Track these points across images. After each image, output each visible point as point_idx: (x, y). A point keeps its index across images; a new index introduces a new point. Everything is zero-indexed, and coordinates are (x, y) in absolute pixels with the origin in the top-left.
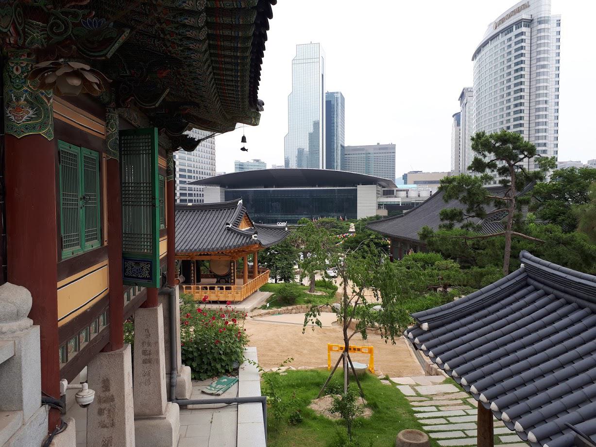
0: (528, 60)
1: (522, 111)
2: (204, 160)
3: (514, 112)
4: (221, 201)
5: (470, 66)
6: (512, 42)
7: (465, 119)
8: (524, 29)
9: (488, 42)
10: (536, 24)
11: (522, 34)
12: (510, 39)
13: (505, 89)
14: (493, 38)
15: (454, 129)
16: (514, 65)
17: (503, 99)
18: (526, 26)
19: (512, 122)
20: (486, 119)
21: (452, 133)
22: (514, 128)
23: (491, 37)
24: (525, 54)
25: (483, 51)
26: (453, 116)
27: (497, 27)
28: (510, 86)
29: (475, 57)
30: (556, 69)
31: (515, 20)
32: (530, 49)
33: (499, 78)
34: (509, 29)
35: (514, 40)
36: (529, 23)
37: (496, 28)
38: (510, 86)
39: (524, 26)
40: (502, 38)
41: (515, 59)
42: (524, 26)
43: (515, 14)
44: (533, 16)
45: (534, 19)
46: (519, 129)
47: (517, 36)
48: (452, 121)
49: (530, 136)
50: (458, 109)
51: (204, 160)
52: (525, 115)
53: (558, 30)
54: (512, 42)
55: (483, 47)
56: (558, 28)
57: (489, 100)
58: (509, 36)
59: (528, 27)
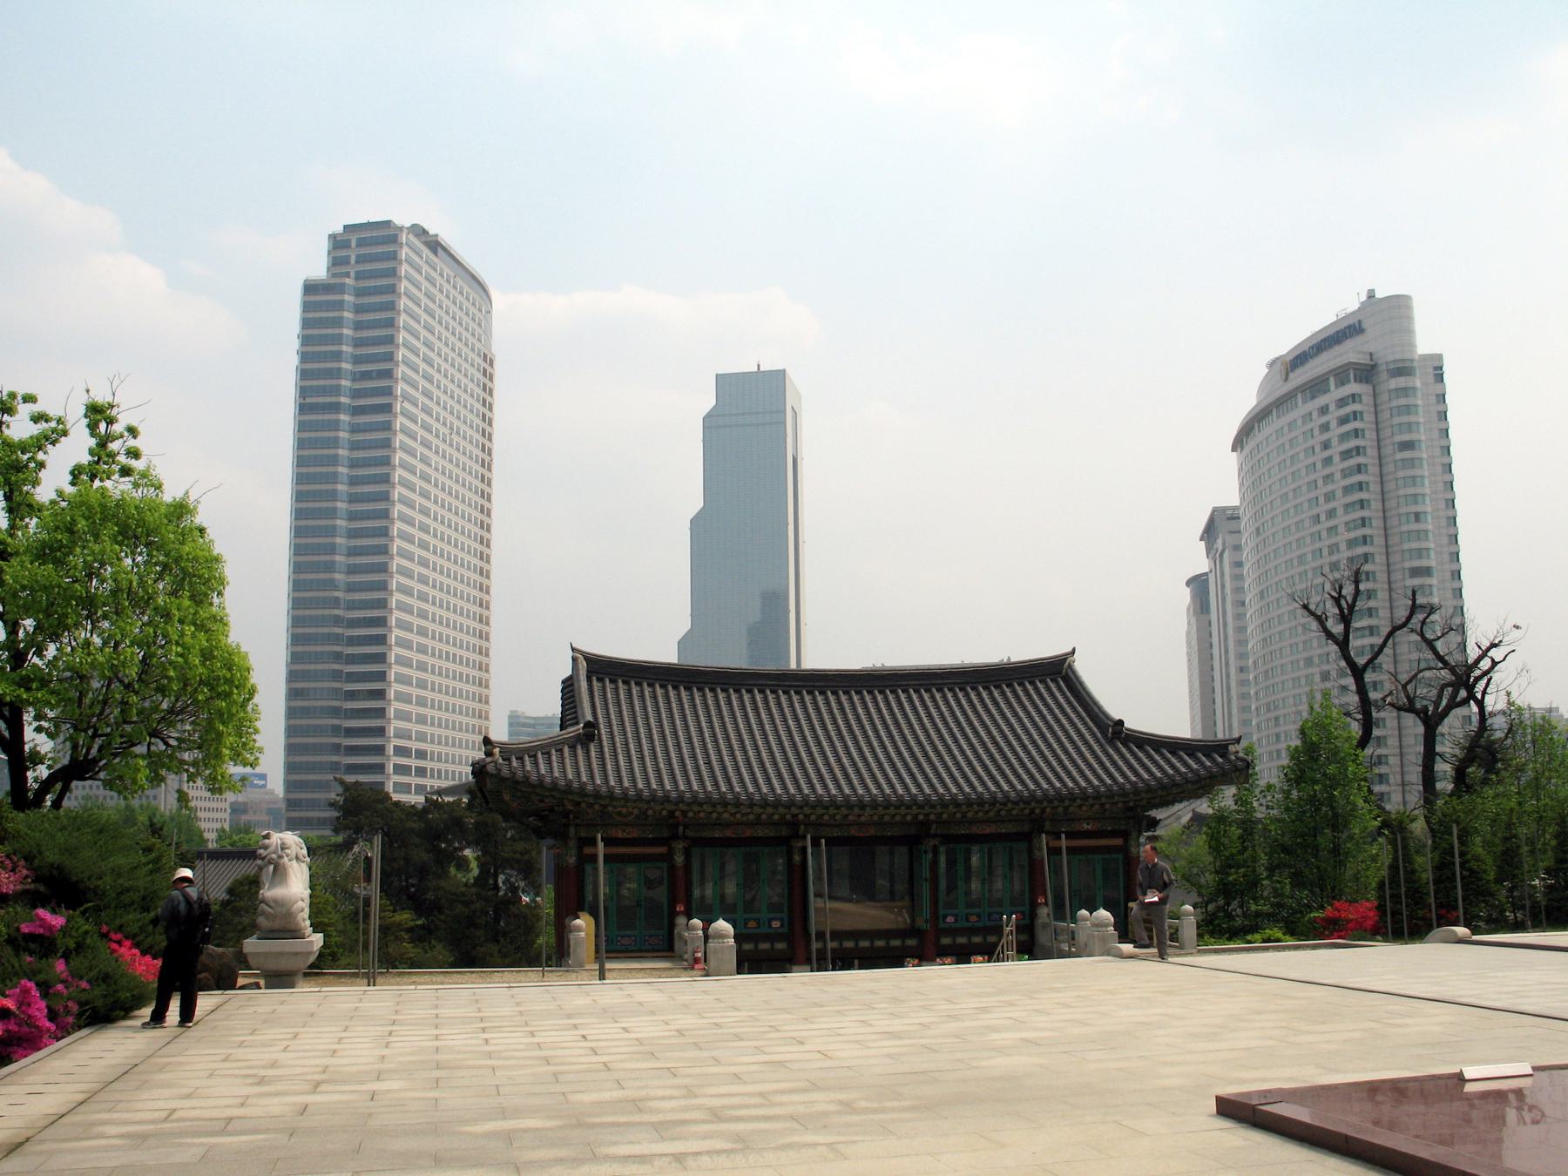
0: (1373, 465)
1: (1364, 485)
2: (458, 718)
3: (1342, 453)
4: (511, 734)
5: (1230, 462)
6: (1338, 504)
7: (1223, 593)
8: (1353, 387)
9: (1253, 427)
10: (1384, 376)
11: (1354, 398)
12: (1324, 410)
13: (1316, 432)
14: (1282, 404)
15: (1193, 621)
16: (1336, 439)
17: (1317, 493)
18: (1358, 380)
19: (1343, 534)
20: (1275, 513)
21: (1188, 633)
22: (1346, 512)
23: (1278, 399)
24: (1367, 483)
25: (1259, 431)
26: (1188, 584)
27: (1292, 376)
28: (1328, 423)
29: (1238, 444)
30: (1442, 452)
31: (1333, 364)
32: (1374, 419)
33: (1303, 473)
34: (1316, 387)
35: (1335, 414)
36: (1367, 372)
37: (1286, 379)
38: (1328, 423)
39: (1355, 381)
40: (1304, 407)
41: (1344, 496)
42: (1355, 381)
43: (1330, 346)
44: (1375, 357)
45: (1379, 362)
46: (1360, 550)
47: (1342, 402)
48: (1185, 596)
49: (1390, 550)
50: (1202, 565)
51: (458, 718)
52: (1381, 604)
53: (1439, 392)
54: (1338, 504)
55: (1259, 421)
56: (1439, 385)
57: (1284, 529)
58: (1322, 400)
59: (1367, 383)
